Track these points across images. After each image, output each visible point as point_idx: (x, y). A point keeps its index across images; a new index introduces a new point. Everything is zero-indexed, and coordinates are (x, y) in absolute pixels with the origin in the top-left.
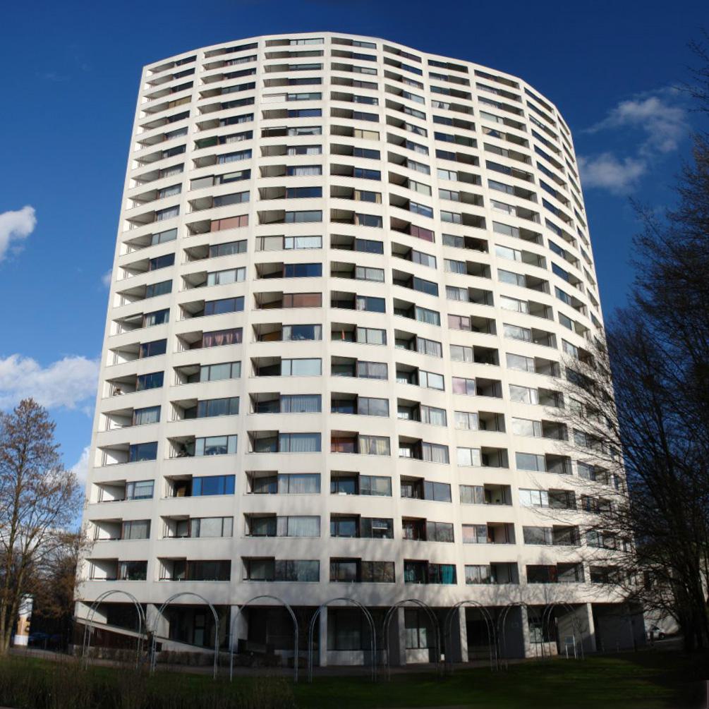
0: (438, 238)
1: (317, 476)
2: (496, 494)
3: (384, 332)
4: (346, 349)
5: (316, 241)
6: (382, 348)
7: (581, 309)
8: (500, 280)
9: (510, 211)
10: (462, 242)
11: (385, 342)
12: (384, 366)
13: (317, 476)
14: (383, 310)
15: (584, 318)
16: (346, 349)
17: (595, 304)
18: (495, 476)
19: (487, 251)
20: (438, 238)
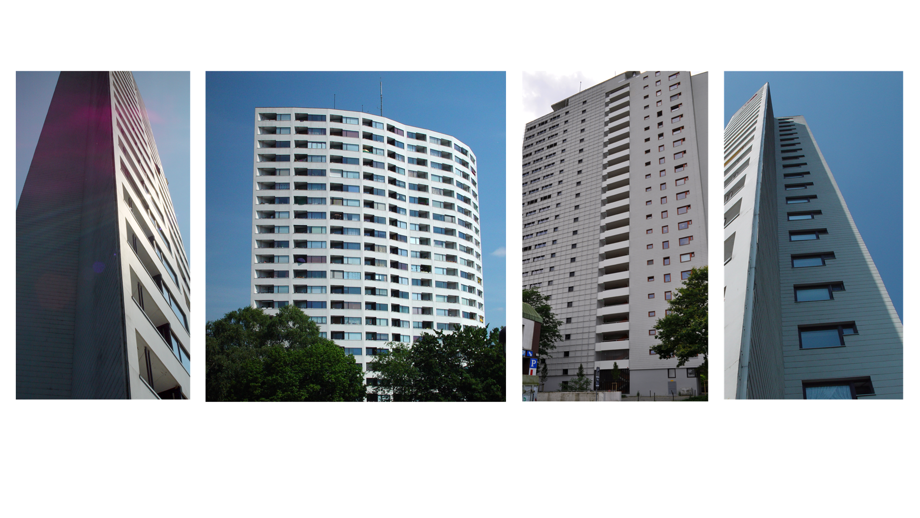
0: (405, 134)
1: (359, 229)
2: (426, 311)
3: (387, 320)
4: (372, 329)
5: (357, 203)
6: (387, 327)
7: (466, 165)
8: (431, 154)
9: (442, 245)
10: (417, 200)
11: (387, 325)
12: (385, 291)
13: (359, 229)
14: (384, 168)
15: (470, 218)
16: (372, 329)
17: (473, 161)
18: (425, 248)
19: (431, 272)
20: (405, 134)
